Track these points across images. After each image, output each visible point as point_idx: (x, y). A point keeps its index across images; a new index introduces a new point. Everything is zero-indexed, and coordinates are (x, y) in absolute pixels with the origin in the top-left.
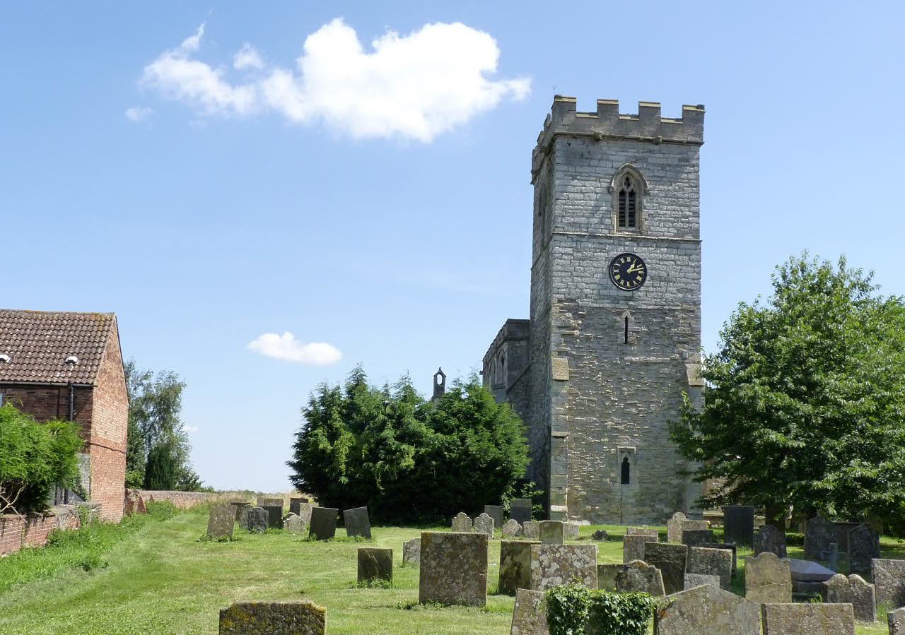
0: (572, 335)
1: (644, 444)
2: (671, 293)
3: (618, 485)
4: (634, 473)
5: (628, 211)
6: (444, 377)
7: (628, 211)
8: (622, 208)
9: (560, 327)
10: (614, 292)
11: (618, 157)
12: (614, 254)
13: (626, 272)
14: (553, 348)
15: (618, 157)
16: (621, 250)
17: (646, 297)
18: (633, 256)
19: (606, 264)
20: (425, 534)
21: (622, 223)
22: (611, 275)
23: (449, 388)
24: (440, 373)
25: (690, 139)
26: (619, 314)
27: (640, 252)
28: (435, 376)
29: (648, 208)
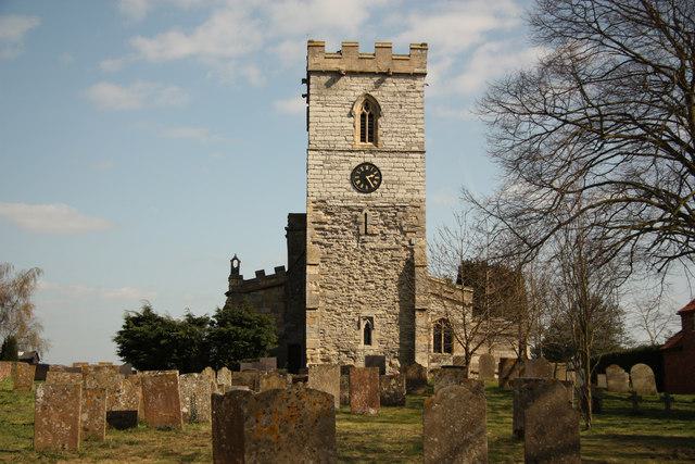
0: (323, 229)
1: (565, 137)
2: (402, 194)
3: (362, 345)
4: (375, 336)
5: (369, 130)
6: (239, 262)
7: (369, 130)
8: (363, 128)
9: (314, 223)
10: (356, 194)
11: (358, 88)
12: (355, 165)
13: (365, 178)
14: (309, 239)
15: (358, 88)
16: (361, 161)
17: (381, 196)
18: (371, 165)
19: (349, 172)
20: (593, 411)
21: (363, 139)
22: (353, 181)
23: (248, 274)
24: (235, 258)
25: (417, 70)
26: (361, 211)
27: (377, 161)
28: (232, 261)
29: (383, 125)
